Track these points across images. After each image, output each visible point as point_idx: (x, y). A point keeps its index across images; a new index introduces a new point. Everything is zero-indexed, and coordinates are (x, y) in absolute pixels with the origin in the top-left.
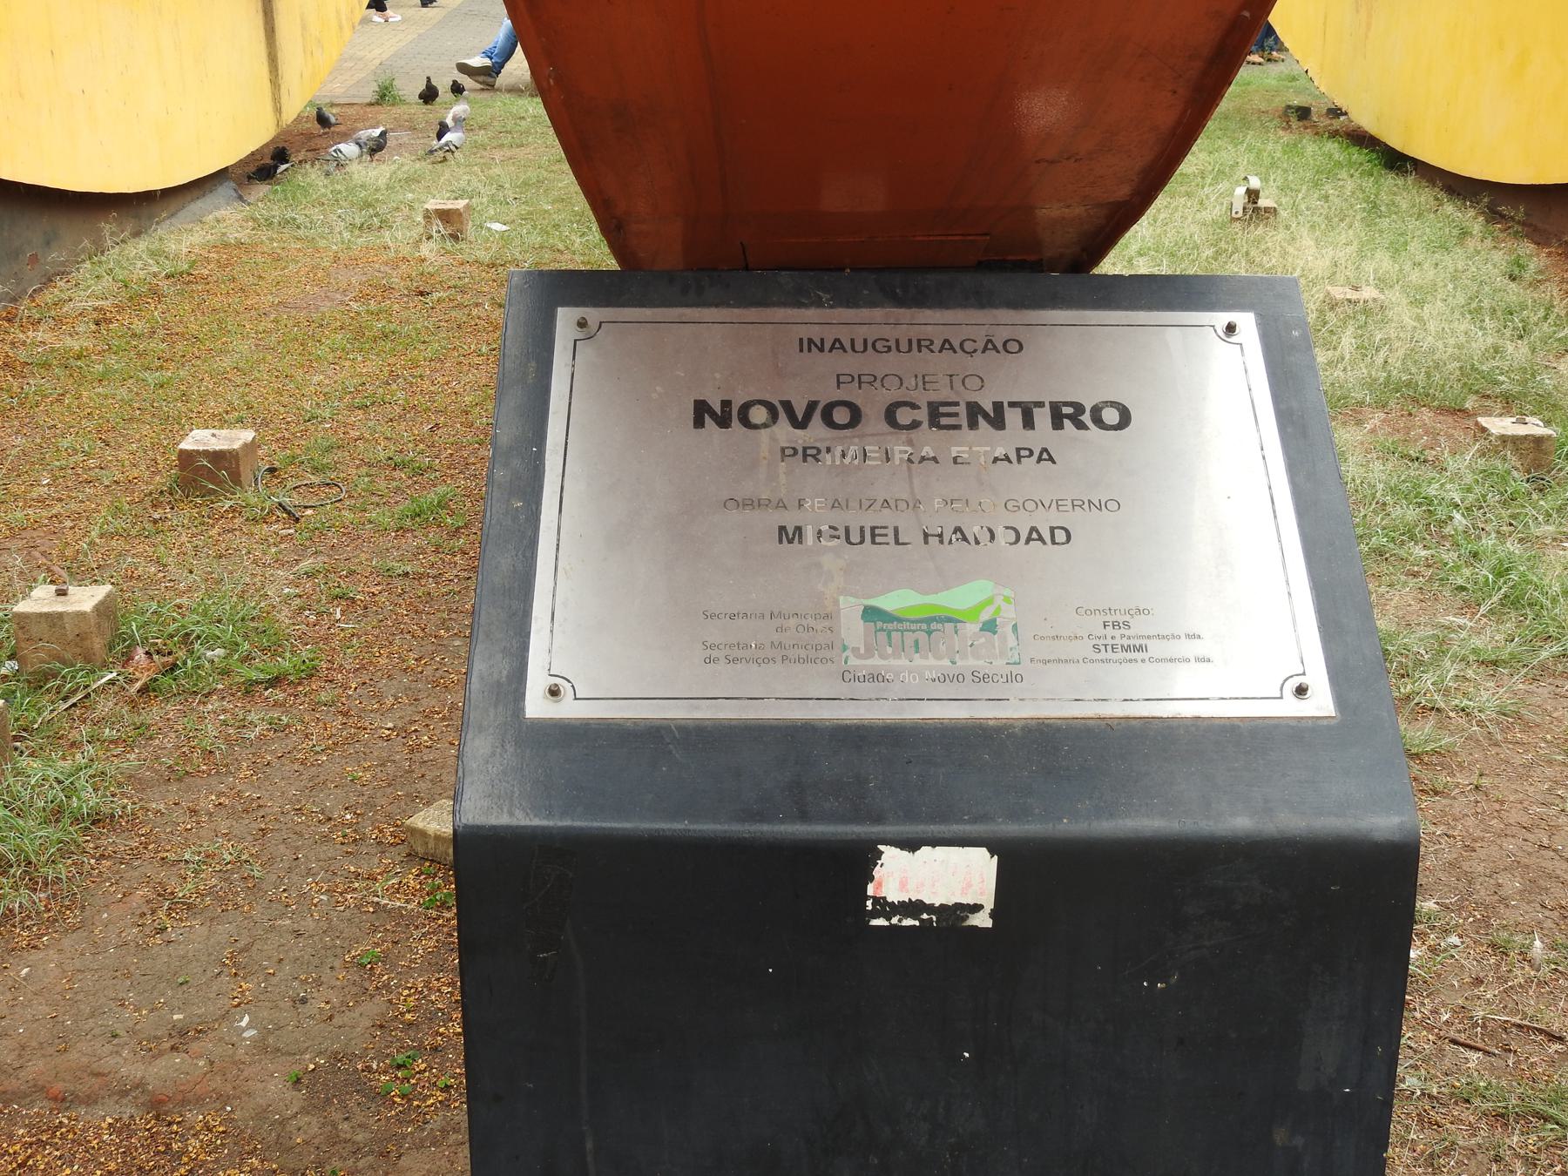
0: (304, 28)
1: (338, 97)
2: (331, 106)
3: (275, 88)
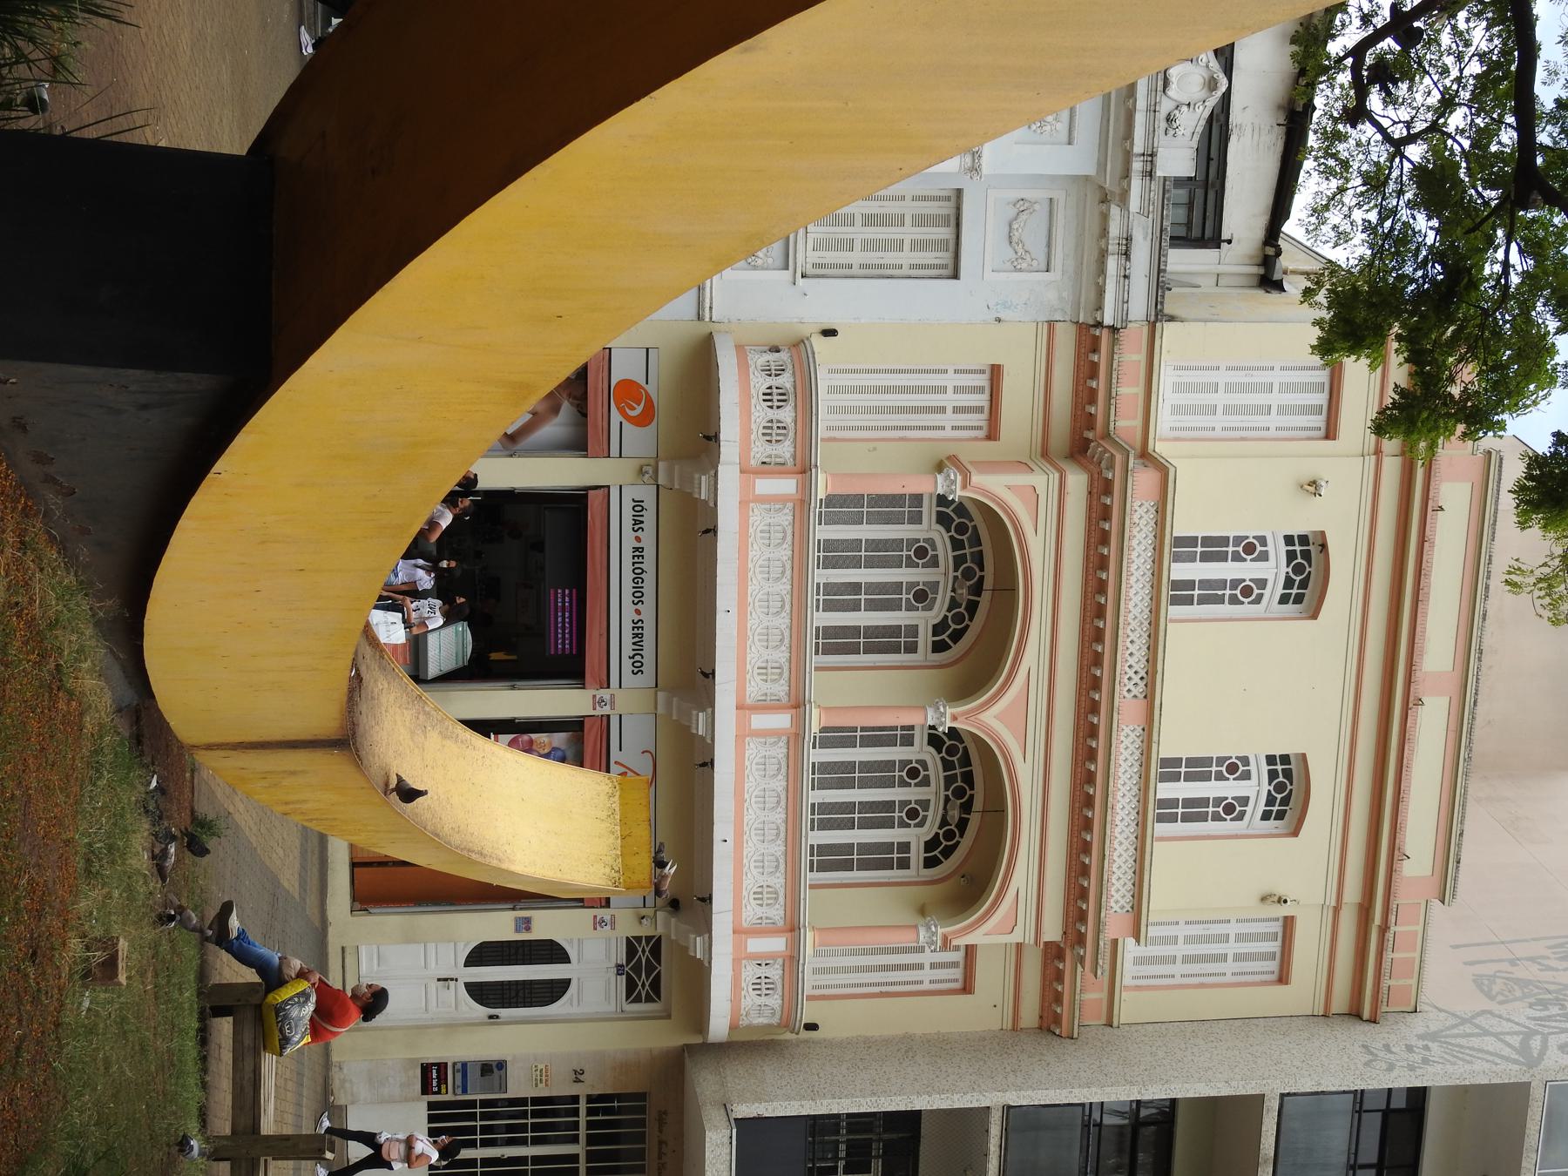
0: (293, 773)
1: (199, 773)
2: (192, 770)
3: (233, 746)
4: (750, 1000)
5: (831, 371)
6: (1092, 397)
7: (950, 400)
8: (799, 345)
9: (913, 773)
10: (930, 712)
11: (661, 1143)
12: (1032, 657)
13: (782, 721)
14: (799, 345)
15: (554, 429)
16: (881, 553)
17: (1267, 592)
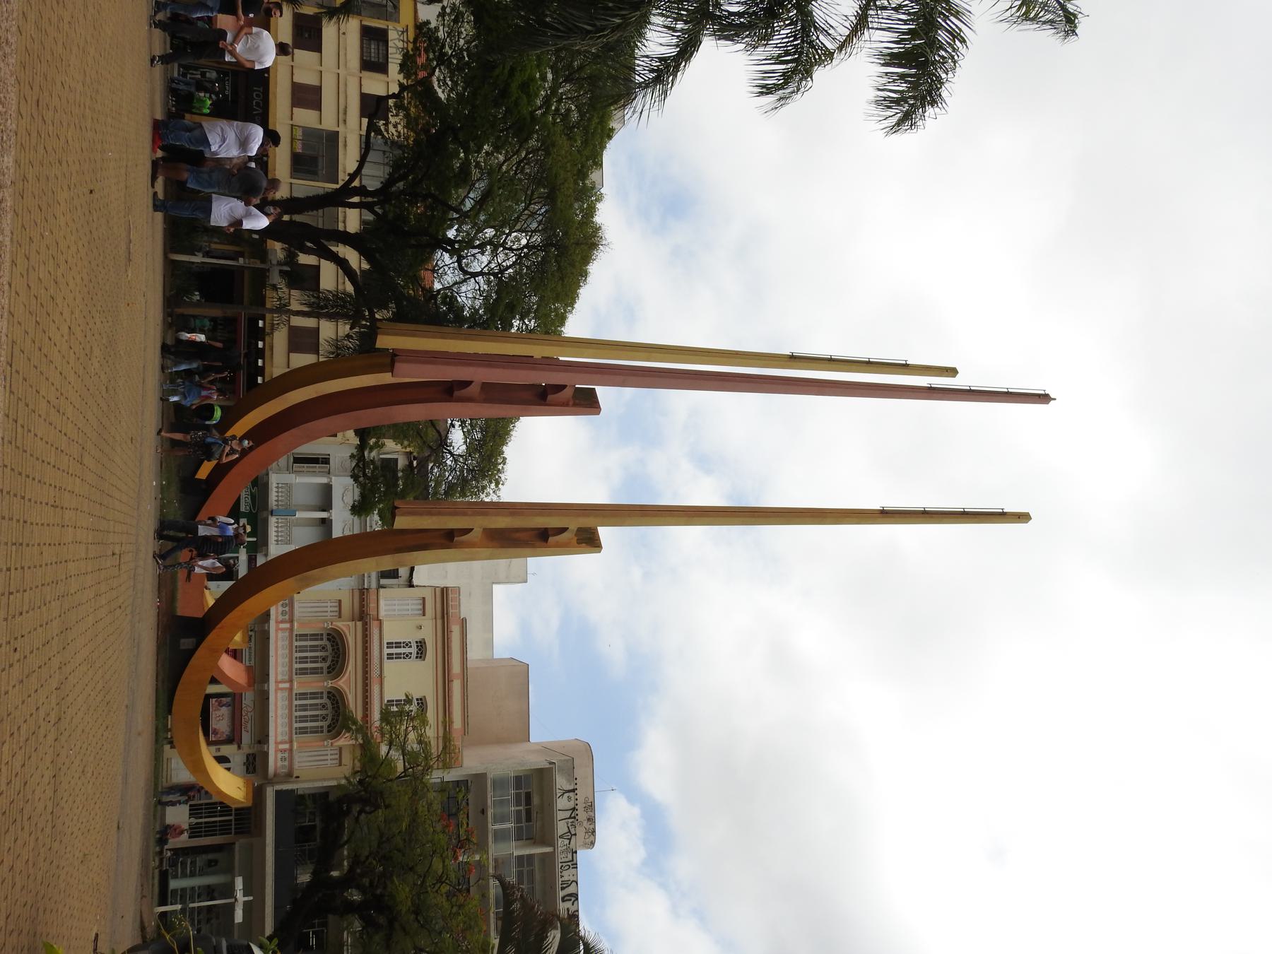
4: (280, 763)
6: (363, 606)
7: (329, 609)
9: (323, 648)
13: (287, 685)
16: (313, 649)
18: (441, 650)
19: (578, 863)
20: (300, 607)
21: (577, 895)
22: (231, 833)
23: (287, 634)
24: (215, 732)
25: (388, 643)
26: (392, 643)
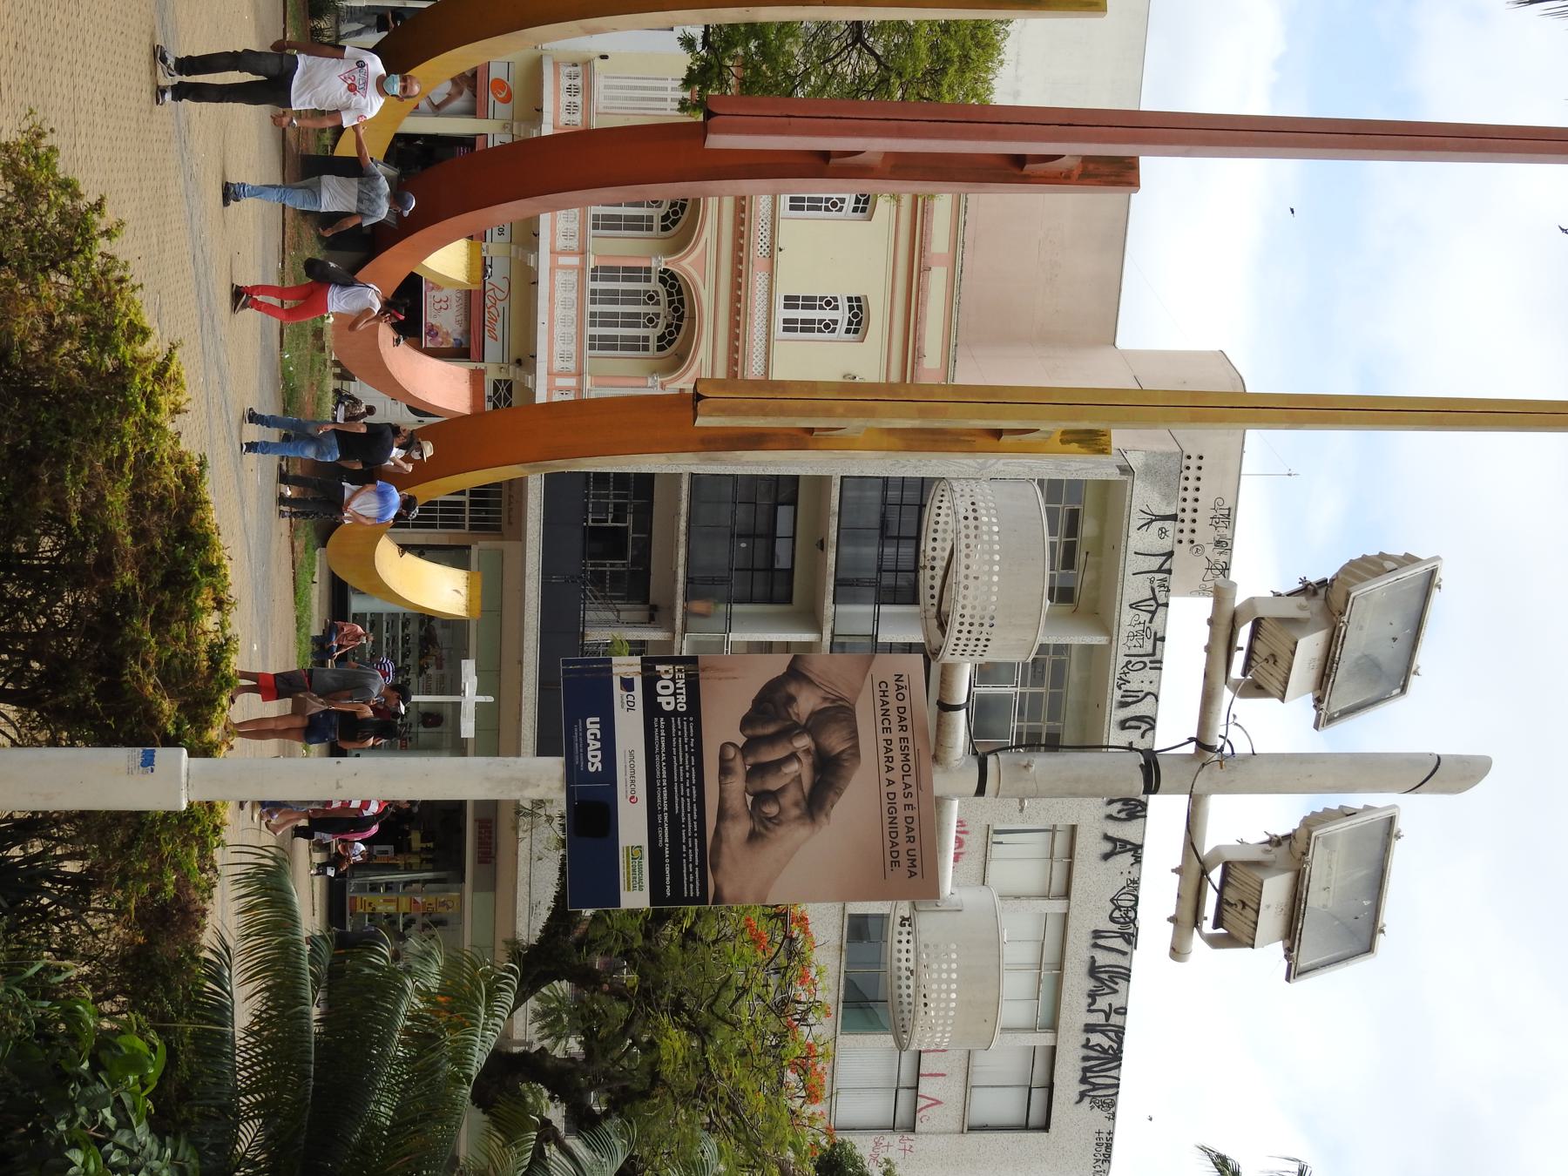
5: (606, 77)
8: (587, 63)
9: (651, 298)
10: (654, 260)
11: (510, 496)
12: (708, 232)
13: (575, 261)
14: (587, 63)
15: (459, 103)
16: (631, 297)
17: (845, 205)
18: (900, 366)
19: (1164, 661)
20: (606, 87)
21: (1154, 721)
22: (463, 527)
23: (573, 277)
24: (433, 332)
25: (787, 298)
26: (797, 298)
